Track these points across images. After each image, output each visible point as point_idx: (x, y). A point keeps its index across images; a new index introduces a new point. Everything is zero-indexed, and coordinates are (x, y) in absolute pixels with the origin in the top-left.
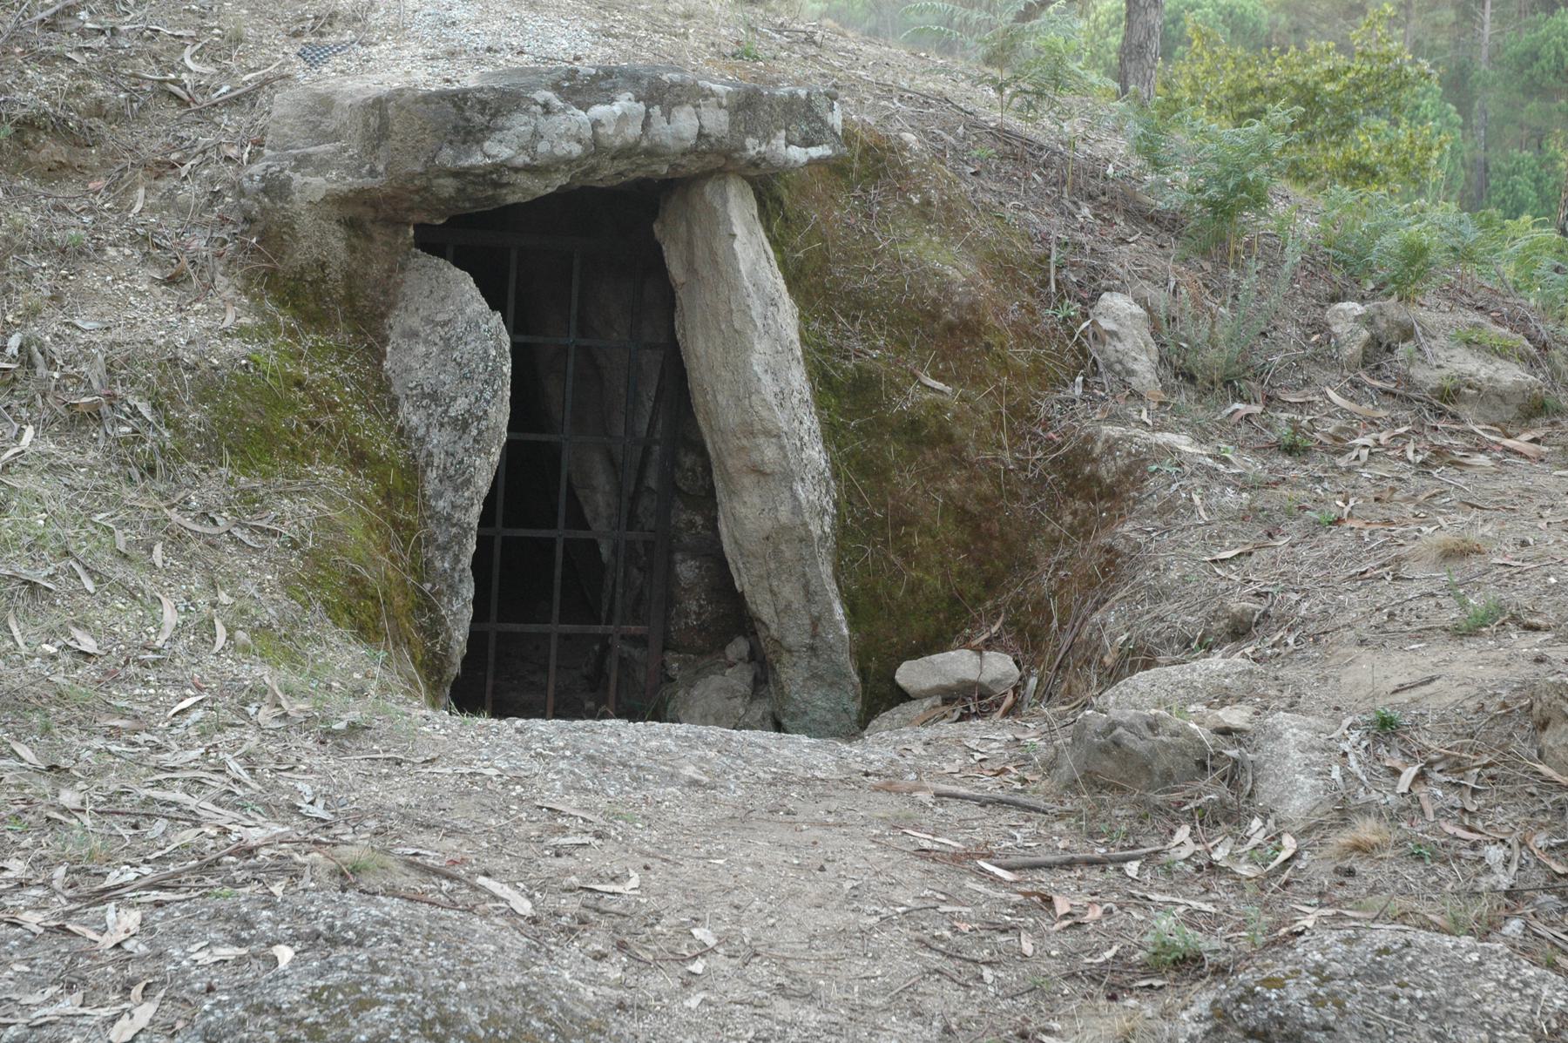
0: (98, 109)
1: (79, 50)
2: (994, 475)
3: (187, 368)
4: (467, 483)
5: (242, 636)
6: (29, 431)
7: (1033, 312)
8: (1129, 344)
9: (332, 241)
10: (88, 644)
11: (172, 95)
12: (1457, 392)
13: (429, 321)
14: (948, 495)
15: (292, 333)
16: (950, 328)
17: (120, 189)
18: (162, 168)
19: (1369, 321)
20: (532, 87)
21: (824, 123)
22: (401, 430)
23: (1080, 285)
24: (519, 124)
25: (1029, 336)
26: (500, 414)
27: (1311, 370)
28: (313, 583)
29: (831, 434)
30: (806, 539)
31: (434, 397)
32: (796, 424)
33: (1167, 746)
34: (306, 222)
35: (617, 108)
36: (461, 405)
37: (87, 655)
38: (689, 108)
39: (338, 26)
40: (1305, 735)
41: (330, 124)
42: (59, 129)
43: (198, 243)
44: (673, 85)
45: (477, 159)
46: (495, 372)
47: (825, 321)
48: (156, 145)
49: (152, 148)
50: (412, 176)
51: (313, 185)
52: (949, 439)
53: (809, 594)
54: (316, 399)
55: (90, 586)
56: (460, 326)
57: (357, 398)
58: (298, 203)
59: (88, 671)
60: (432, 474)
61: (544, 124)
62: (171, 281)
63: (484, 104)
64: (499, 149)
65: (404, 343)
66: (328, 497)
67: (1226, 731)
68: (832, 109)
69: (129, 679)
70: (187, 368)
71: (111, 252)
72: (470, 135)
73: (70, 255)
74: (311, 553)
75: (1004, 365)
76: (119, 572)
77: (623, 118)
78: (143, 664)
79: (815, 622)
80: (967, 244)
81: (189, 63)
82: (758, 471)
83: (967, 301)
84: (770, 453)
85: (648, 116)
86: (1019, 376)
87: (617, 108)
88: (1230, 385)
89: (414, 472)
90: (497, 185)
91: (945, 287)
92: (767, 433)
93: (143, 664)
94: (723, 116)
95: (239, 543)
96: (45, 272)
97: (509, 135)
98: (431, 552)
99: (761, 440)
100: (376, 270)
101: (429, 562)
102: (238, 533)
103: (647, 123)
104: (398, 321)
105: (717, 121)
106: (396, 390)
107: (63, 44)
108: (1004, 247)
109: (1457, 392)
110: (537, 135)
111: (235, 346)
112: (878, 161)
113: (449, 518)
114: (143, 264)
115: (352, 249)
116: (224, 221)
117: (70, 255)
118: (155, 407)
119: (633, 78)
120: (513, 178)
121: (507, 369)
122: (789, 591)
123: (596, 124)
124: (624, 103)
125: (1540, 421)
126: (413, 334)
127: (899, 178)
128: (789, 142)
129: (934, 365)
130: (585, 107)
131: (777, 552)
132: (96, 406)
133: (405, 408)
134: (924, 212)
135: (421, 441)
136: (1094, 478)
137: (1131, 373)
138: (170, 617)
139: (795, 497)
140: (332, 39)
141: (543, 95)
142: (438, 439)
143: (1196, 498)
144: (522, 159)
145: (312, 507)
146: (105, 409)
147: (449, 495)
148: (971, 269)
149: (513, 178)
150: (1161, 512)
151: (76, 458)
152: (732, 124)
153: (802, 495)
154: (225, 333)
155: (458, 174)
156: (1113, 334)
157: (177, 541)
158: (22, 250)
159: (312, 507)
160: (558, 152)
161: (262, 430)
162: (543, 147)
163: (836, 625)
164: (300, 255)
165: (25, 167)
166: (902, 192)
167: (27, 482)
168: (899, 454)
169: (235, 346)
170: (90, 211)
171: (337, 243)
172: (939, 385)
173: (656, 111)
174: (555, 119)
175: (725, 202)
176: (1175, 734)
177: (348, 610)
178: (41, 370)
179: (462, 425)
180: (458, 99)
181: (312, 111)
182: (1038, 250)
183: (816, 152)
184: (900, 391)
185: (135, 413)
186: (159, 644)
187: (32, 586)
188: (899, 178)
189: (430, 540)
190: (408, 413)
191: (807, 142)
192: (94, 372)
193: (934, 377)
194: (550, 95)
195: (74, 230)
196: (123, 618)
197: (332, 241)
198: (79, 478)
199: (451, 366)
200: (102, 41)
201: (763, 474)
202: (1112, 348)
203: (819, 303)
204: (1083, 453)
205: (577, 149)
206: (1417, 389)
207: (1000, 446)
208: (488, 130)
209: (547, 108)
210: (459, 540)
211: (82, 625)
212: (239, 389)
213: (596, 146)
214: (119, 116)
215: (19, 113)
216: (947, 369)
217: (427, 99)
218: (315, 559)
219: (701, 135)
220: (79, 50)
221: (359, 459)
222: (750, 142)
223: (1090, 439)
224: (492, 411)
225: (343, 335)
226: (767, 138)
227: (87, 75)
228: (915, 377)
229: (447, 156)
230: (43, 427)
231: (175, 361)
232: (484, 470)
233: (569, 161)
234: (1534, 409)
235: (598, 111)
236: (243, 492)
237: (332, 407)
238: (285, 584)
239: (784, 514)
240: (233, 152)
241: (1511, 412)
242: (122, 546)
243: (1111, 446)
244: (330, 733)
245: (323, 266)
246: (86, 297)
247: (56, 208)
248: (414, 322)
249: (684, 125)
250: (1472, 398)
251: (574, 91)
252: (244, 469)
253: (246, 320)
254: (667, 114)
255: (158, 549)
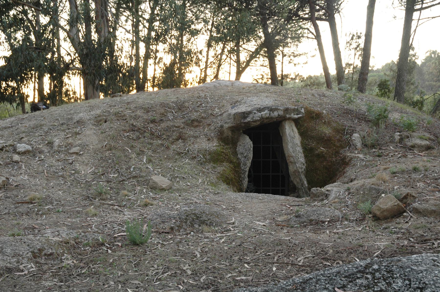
0: (202, 118)
1: (201, 110)
2: (331, 162)
3: (208, 151)
4: (246, 165)
5: (209, 183)
6: (187, 160)
7: (342, 137)
8: (357, 141)
9: (229, 133)
10: (189, 184)
11: (213, 115)
12: (414, 146)
13: (242, 143)
14: (324, 165)
15: (223, 146)
16: (326, 140)
17: (204, 128)
18: (209, 125)
19: (400, 135)
20: (253, 111)
21: (301, 112)
22: (238, 158)
23: (351, 132)
24: (251, 116)
25: (340, 141)
26: (251, 155)
27: (388, 144)
28: (221, 178)
29: (306, 157)
30: (299, 172)
31: (242, 154)
32: (297, 155)
33: (319, 192)
34: (226, 131)
35: (265, 112)
36: (245, 154)
37: (188, 185)
38: (276, 111)
39: (238, 102)
40: (336, 190)
41: (230, 117)
42: (197, 121)
43: (212, 135)
44: (274, 108)
45: (246, 121)
46: (250, 150)
47: (307, 140)
48: (209, 122)
49: (209, 122)
50: (238, 124)
51: (226, 126)
52: (324, 157)
53: (301, 180)
54: (225, 154)
55: (191, 178)
56: (246, 143)
57: (232, 154)
58: (224, 128)
59: (189, 187)
60: (242, 164)
61: (254, 115)
62: (208, 140)
63: (247, 113)
64: (249, 119)
65: (239, 146)
66: (225, 167)
67: (327, 190)
68: (302, 109)
69: (193, 188)
70: (208, 151)
71: (201, 136)
72: (245, 118)
73: (196, 137)
74: (221, 174)
75: (335, 145)
76: (195, 176)
77: (266, 114)
78: (195, 186)
79: (302, 184)
80: (331, 127)
81: (216, 110)
82: (291, 162)
83: (328, 136)
84: (292, 159)
85: (270, 113)
86: (337, 147)
87: (265, 112)
88: (373, 146)
89: (239, 164)
90: (249, 124)
91: (325, 134)
92: (291, 157)
93: (195, 186)
94: (282, 112)
95: (212, 173)
96: (192, 139)
97: (250, 117)
98: (241, 174)
99: (291, 158)
100: (236, 137)
101: (241, 176)
102: (212, 172)
103: (270, 114)
104: (239, 143)
105: (281, 113)
106: (238, 153)
107: (199, 109)
108: (338, 127)
109: (414, 146)
110: (253, 117)
111: (215, 148)
112: (318, 116)
113: (243, 170)
114: (205, 138)
115: (232, 134)
116: (216, 131)
117: (196, 137)
118: (203, 156)
119: (268, 108)
120: (251, 123)
121: (252, 149)
122: (298, 180)
123: (262, 115)
124: (266, 111)
125: (429, 150)
126: (240, 145)
127: (321, 118)
128: (294, 115)
129: (323, 146)
130: (260, 113)
131: (295, 174)
132: (196, 156)
133: (239, 155)
134: (325, 123)
135: (240, 160)
136: (346, 161)
137: (357, 146)
138: (200, 181)
139: (296, 166)
140: (236, 105)
141: (254, 111)
142: (243, 159)
143: (358, 164)
144: (252, 120)
145: (222, 168)
146: (197, 157)
147: (244, 167)
148: (330, 131)
149: (251, 123)
150: (353, 166)
151: (192, 163)
152: (284, 113)
153: (297, 165)
154: (214, 146)
155: (244, 123)
156: (354, 140)
157: (204, 172)
158: (190, 137)
159: (222, 168)
160: (256, 119)
161: (217, 159)
162: (254, 119)
163: (305, 185)
164: (225, 135)
165: (193, 126)
166: (322, 120)
167: (186, 166)
168: (316, 159)
169: (215, 148)
170: (200, 131)
171: (230, 133)
172: (323, 149)
173: (271, 112)
174: (256, 115)
175: (285, 124)
176: (320, 191)
177: (226, 181)
178: (190, 152)
179: (245, 157)
180: (244, 113)
181: (228, 115)
182: (344, 127)
183: (299, 116)
184: (317, 150)
185: (201, 157)
186: (366, 249)
187: (184, 178)
188: (321, 118)
189: (241, 173)
190: (239, 156)
191: (297, 114)
192: (196, 152)
193: (323, 148)
194: (255, 111)
195: (197, 134)
196: (194, 181)
197: (229, 133)
198: (192, 165)
199: (244, 149)
200: (205, 108)
201: (292, 163)
202: (354, 142)
203: (306, 138)
204: (345, 158)
205: (259, 118)
206: (407, 146)
207: (333, 157)
208: (247, 117)
209: (255, 113)
210: (245, 172)
211: (189, 182)
212: (214, 153)
213: (262, 118)
214: (205, 118)
215: (192, 119)
216: (325, 146)
217: (240, 113)
218: (222, 175)
219: (279, 115)
220: (201, 110)
221: (231, 162)
222: (287, 115)
223: (346, 156)
224: (249, 155)
225: (231, 146)
226: (290, 114)
227: (202, 113)
228: (319, 148)
229: (242, 121)
230: (189, 159)
231: (206, 150)
232: (249, 164)
233: (258, 120)
234: (428, 148)
235: (262, 113)
236: (214, 167)
237: (228, 155)
238: (217, 178)
239: (295, 168)
240: (218, 122)
241: (424, 149)
242: (196, 173)
243: (348, 156)
244: (215, 193)
245: (228, 137)
246: (196, 143)
247: (195, 131)
248: (241, 143)
249: (276, 114)
250: (417, 147)
251: (260, 110)
252: (214, 164)
253: (217, 144)
254: (273, 113)
255: (201, 174)
